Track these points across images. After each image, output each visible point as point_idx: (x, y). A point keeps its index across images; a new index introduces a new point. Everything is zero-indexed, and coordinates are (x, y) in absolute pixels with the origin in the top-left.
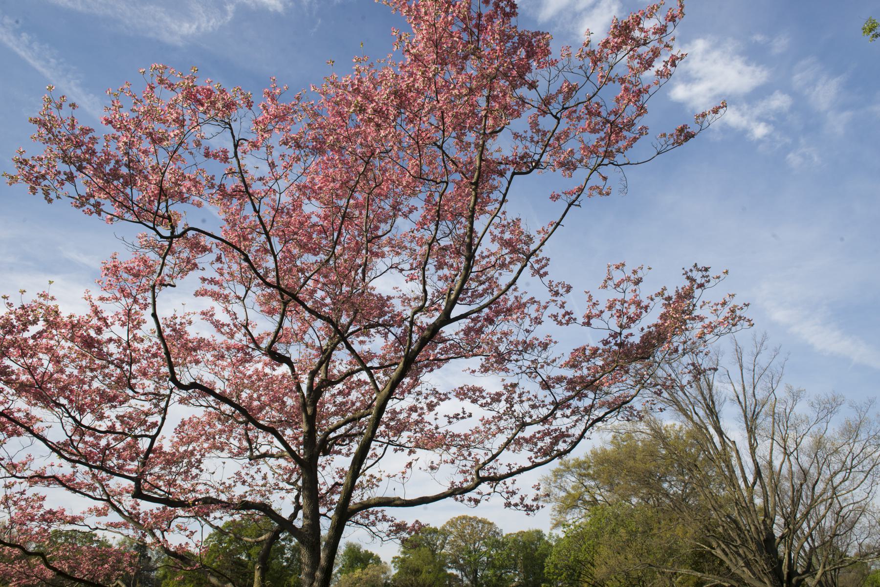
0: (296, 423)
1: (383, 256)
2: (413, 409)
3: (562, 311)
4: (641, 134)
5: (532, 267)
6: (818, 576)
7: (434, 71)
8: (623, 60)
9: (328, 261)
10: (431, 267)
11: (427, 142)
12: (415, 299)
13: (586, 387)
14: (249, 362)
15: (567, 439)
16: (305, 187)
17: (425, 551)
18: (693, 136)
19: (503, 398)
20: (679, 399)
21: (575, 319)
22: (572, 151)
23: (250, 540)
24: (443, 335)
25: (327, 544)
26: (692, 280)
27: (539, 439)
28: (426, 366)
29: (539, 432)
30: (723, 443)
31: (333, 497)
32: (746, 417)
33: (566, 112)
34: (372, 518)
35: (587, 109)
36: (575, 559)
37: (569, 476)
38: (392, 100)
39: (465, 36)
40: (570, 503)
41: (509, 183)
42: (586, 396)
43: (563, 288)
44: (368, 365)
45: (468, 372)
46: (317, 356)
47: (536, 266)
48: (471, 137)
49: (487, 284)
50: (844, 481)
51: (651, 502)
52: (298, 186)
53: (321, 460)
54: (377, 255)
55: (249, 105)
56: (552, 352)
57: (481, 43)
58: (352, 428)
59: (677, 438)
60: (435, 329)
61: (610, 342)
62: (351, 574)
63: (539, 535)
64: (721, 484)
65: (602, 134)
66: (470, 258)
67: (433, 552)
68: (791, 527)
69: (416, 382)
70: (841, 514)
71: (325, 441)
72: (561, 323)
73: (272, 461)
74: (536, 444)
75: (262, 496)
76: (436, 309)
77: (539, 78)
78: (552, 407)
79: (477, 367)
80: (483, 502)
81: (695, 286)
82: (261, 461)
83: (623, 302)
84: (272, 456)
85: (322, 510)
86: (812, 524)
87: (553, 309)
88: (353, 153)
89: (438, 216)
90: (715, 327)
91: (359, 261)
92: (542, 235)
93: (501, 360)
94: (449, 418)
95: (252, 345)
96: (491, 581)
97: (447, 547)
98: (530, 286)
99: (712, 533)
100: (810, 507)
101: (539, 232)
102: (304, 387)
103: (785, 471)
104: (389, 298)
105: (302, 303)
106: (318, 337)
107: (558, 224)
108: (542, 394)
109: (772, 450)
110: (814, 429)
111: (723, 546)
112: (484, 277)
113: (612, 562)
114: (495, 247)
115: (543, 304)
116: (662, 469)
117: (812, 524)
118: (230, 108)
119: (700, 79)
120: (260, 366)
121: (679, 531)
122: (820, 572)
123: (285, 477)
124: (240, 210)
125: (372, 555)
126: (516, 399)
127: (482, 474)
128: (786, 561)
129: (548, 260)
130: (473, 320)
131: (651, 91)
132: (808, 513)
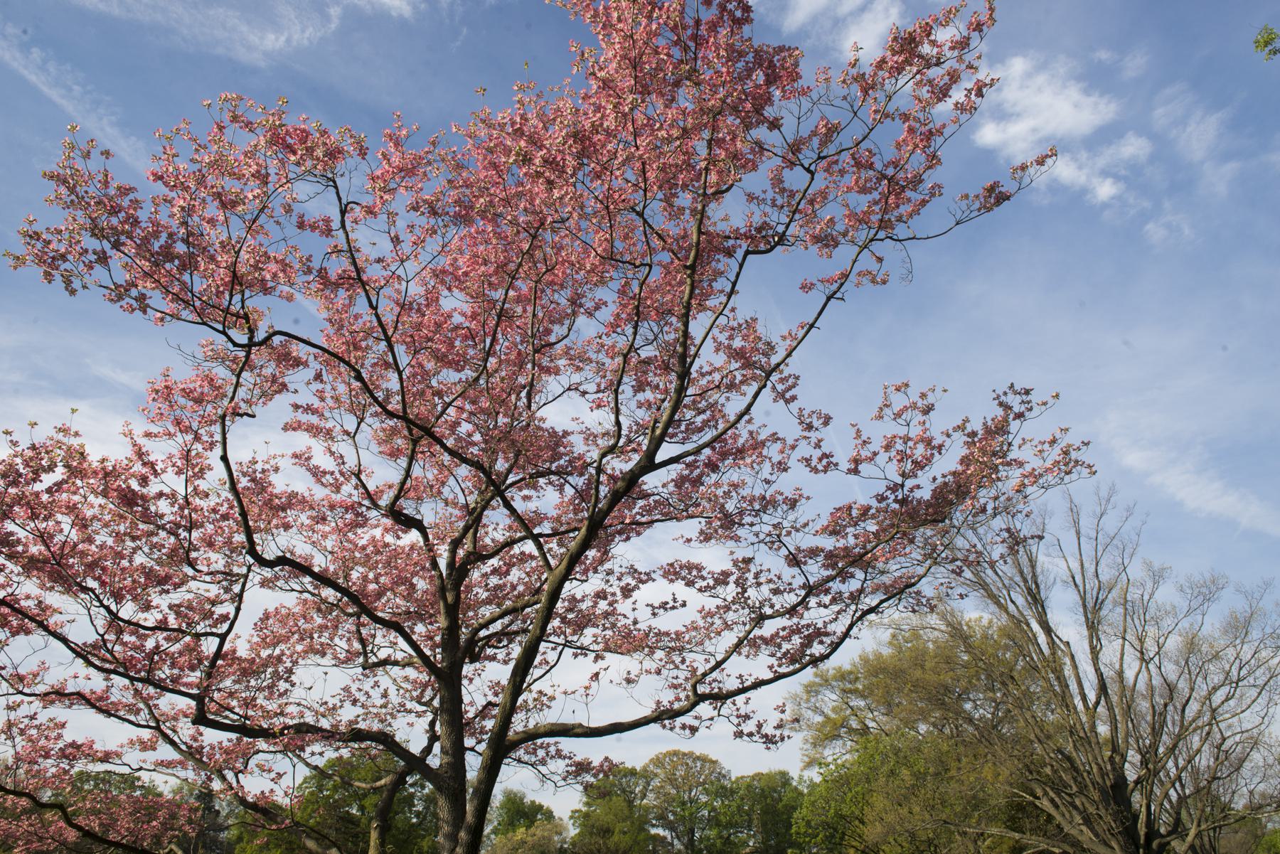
0: (431, 616)
1: (557, 372)
2: (601, 595)
3: (818, 453)
4: (933, 195)
5: (774, 388)
6: (1189, 839)
7: (632, 103)
8: (906, 88)
9: (477, 379)
10: (627, 389)
11: (621, 206)
12: (604, 435)
13: (852, 564)
14: (362, 526)
15: (825, 639)
16: (444, 272)
17: (618, 802)
18: (1008, 198)
19: (732, 579)
20: (988, 581)
21: (836, 465)
22: (832, 220)
23: (364, 785)
24: (645, 487)
25: (476, 791)
26: (1006, 407)
27: (784, 638)
28: (620, 533)
29: (784, 629)
30: (1052, 644)
31: (484, 723)
32: (1085, 606)
33: (824, 163)
34: (541, 753)
35: (854, 159)
36: (836, 813)
37: (827, 693)
38: (571, 146)
39: (677, 53)
40: (830, 732)
41: (741, 266)
42: (853, 576)
43: (818, 418)
44: (536, 531)
45: (681, 541)
46: (460, 518)
47: (780, 387)
48: (685, 199)
49: (708, 413)
50: (1227, 699)
51: (947, 731)
52: (434, 271)
53: (467, 669)
54: (548, 371)
55: (363, 153)
56: (804, 512)
57: (699, 62)
58: (512, 623)
59: (985, 637)
60: (632, 479)
61: (887, 498)
62: (510, 835)
63: (784, 778)
64: (1048, 704)
65: (876, 195)
66: (684, 375)
67: (630, 803)
68: (1151, 766)
69: (605, 556)
70: (1223, 748)
71: (472, 641)
72: (815, 470)
73: (395, 671)
74: (780, 646)
75: (382, 721)
76: (634, 450)
77: (784, 113)
78: (803, 593)
79: (694, 534)
80: (702, 730)
81: (1012, 416)
82: (380, 671)
83: (906, 439)
84: (396, 663)
85: (469, 742)
86: (1181, 763)
87: (804, 450)
88: (514, 222)
89: (638, 314)
90: (1041, 475)
91: (522, 380)
92: (788, 342)
94: (654, 608)
95: (366, 502)
96: (714, 845)
97: (651, 796)
98: (771, 416)
99: (1035, 776)
100: (1179, 738)
101: (784, 338)
102: (443, 564)
103: (1141, 686)
104: (566, 434)
105: (439, 441)
106: (463, 491)
107: (812, 326)
108: (789, 573)
109: (1122, 655)
110: (1185, 624)
111: (1052, 794)
112: (704, 402)
113: (890, 818)
114: (720, 359)
115: (790, 442)
116: (963, 683)
117: (1181, 763)
118: (335, 158)
119: (1018, 115)
120: (377, 533)
121: (987, 772)
122: (1192, 833)
123: (415, 694)
124: (350, 305)
125: (541, 807)
126: (751, 580)
127: (701, 689)
128: (1143, 817)
129: (797, 378)
130: (688, 465)
131: (947, 132)
132: (1175, 746)
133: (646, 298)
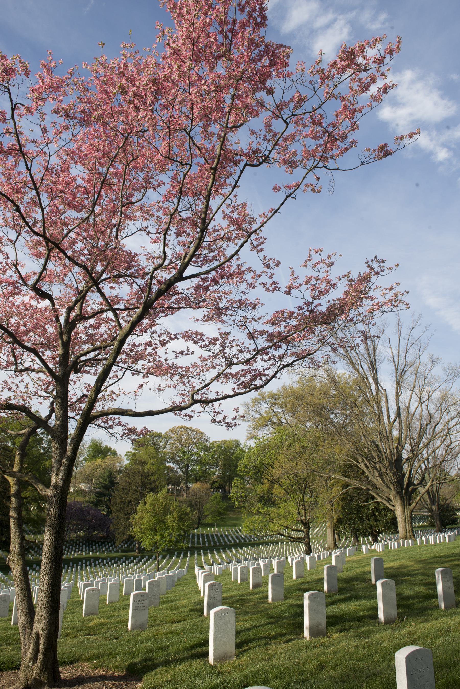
1: (135, 219)
2: (149, 344)
3: (270, 281)
4: (351, 146)
5: (252, 243)
6: (427, 487)
7: (189, 66)
8: (345, 82)
9: (88, 218)
10: (172, 235)
11: (178, 128)
12: (158, 258)
13: (281, 341)
15: (263, 377)
16: (73, 152)
17: (151, 449)
18: (391, 154)
19: (218, 342)
20: (351, 355)
21: (279, 288)
22: (295, 152)
23: (13, 432)
24: (177, 289)
25: (73, 440)
26: (371, 268)
27: (242, 375)
28: (162, 312)
29: (242, 370)
30: (378, 390)
31: (81, 405)
32: (397, 373)
33: (295, 119)
34: (110, 422)
35: (312, 118)
36: (260, 462)
37: (264, 404)
38: (151, 87)
39: (221, 38)
40: (263, 423)
41: (242, 172)
42: (281, 347)
43: (274, 262)
44: (116, 306)
45: (193, 320)
46: (74, 295)
47: (255, 243)
48: (215, 128)
49: (216, 252)
50: (456, 425)
51: (320, 427)
52: (66, 151)
53: (73, 376)
54: (130, 218)
55: (27, 73)
56: (260, 311)
58: (99, 354)
59: (346, 383)
60: (170, 284)
61: (303, 309)
62: (93, 462)
63: (237, 444)
64: (371, 419)
65: (321, 142)
66: (204, 229)
67: (157, 450)
68: (415, 452)
69: (153, 324)
70: (451, 447)
71: (76, 363)
72: (268, 290)
73: (33, 374)
74: (239, 379)
75: (24, 400)
76: (173, 268)
77: (276, 85)
78: (254, 353)
79: (200, 317)
80: (195, 417)
81: (373, 273)
82: (25, 374)
83: (317, 279)
84: (33, 370)
85: (71, 414)
86: (430, 452)
87: (264, 279)
89: (181, 192)
90: (382, 306)
91: (114, 221)
92: (262, 218)
93: (218, 313)
94: (176, 353)
95: (20, 281)
96: (198, 473)
97: (168, 447)
98: (248, 257)
99: (359, 452)
100: (430, 440)
101: (260, 216)
102: (62, 319)
103: (417, 414)
104: (136, 255)
105: (63, 251)
106: (76, 280)
107: (276, 211)
108: (248, 342)
109: (411, 398)
110: (443, 386)
111: (366, 461)
112: (214, 246)
113: (286, 466)
114: (225, 224)
115: (258, 273)
116: (332, 405)
117: (430, 452)
118: (10, 74)
119: (404, 104)
120: (27, 299)
121: (337, 449)
122: (429, 485)
123: (43, 387)
124: (15, 166)
125: (110, 449)
126: (228, 344)
127: (196, 397)
128: (407, 476)
129: (265, 239)
130: (202, 279)
131: (364, 111)
132: (428, 444)
133: (187, 184)
